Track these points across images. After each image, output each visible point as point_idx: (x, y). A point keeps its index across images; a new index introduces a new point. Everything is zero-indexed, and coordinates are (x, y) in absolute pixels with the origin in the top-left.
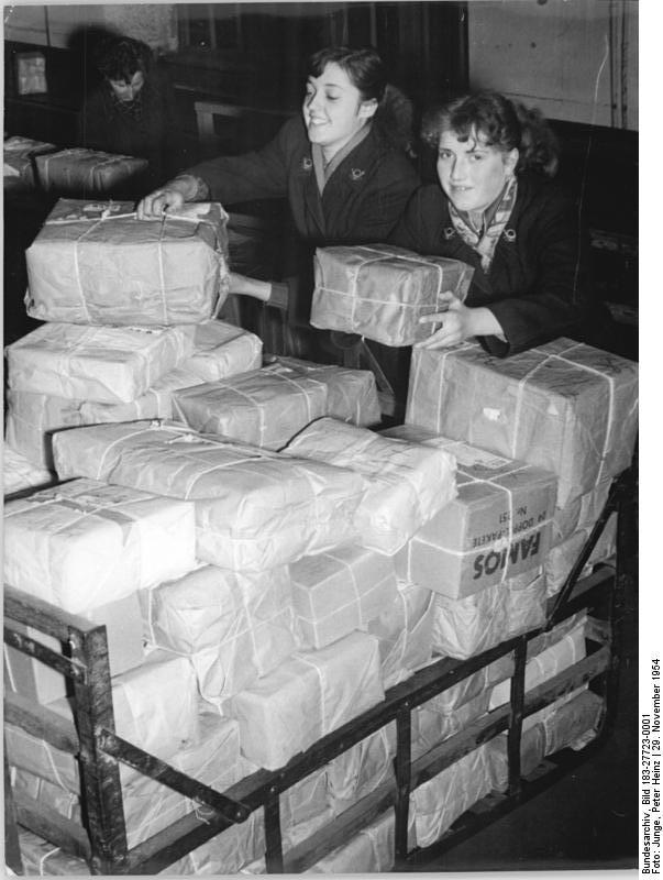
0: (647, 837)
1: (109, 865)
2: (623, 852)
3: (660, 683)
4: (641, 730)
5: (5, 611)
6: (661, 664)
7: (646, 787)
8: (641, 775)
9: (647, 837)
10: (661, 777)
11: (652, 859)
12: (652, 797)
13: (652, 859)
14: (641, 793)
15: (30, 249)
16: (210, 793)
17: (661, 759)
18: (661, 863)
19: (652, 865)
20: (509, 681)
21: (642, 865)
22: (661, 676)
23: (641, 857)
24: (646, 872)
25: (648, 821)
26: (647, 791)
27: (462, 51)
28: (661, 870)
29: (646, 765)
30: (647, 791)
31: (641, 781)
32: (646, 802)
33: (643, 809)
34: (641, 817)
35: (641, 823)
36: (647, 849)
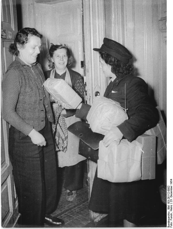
0: (169, 218)
1: (63, 194)
2: (163, 223)
3: (172, 185)
4: (167, 190)
5: (89, 110)
6: (172, 180)
7: (169, 205)
8: (167, 202)
9: (169, 218)
10: (172, 209)
11: (170, 224)
12: (170, 188)
13: (170, 224)
14: (167, 206)
15: (111, 68)
16: (166, 28)
17: (172, 204)
18: (172, 225)
19: (170, 225)
20: (145, 133)
21: (167, 225)
22: (172, 183)
23: (167, 223)
24: (169, 227)
25: (169, 214)
26: (169, 206)
27: (3, 18)
28: (172, 226)
29: (169, 199)
30: (169, 206)
31: (167, 203)
32: (169, 209)
33: (168, 211)
34: (167, 212)
35: (167, 214)
36: (169, 221)
